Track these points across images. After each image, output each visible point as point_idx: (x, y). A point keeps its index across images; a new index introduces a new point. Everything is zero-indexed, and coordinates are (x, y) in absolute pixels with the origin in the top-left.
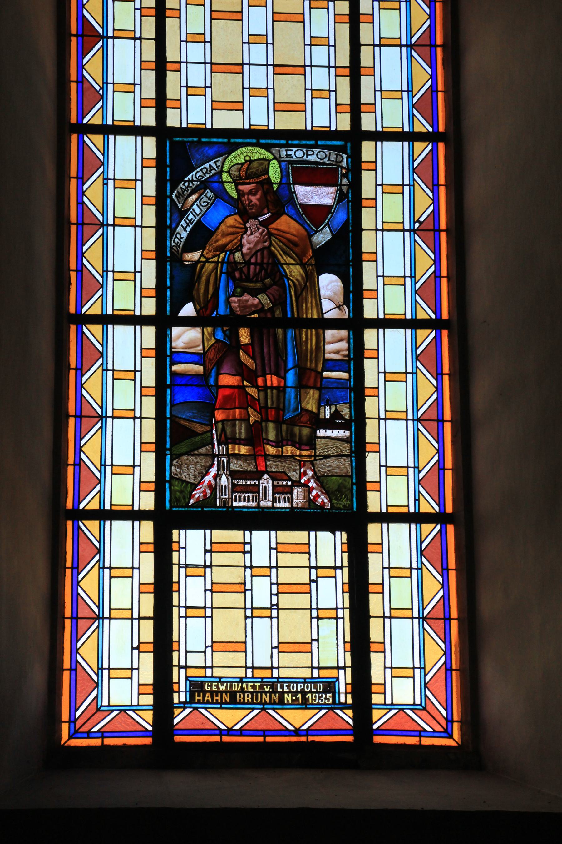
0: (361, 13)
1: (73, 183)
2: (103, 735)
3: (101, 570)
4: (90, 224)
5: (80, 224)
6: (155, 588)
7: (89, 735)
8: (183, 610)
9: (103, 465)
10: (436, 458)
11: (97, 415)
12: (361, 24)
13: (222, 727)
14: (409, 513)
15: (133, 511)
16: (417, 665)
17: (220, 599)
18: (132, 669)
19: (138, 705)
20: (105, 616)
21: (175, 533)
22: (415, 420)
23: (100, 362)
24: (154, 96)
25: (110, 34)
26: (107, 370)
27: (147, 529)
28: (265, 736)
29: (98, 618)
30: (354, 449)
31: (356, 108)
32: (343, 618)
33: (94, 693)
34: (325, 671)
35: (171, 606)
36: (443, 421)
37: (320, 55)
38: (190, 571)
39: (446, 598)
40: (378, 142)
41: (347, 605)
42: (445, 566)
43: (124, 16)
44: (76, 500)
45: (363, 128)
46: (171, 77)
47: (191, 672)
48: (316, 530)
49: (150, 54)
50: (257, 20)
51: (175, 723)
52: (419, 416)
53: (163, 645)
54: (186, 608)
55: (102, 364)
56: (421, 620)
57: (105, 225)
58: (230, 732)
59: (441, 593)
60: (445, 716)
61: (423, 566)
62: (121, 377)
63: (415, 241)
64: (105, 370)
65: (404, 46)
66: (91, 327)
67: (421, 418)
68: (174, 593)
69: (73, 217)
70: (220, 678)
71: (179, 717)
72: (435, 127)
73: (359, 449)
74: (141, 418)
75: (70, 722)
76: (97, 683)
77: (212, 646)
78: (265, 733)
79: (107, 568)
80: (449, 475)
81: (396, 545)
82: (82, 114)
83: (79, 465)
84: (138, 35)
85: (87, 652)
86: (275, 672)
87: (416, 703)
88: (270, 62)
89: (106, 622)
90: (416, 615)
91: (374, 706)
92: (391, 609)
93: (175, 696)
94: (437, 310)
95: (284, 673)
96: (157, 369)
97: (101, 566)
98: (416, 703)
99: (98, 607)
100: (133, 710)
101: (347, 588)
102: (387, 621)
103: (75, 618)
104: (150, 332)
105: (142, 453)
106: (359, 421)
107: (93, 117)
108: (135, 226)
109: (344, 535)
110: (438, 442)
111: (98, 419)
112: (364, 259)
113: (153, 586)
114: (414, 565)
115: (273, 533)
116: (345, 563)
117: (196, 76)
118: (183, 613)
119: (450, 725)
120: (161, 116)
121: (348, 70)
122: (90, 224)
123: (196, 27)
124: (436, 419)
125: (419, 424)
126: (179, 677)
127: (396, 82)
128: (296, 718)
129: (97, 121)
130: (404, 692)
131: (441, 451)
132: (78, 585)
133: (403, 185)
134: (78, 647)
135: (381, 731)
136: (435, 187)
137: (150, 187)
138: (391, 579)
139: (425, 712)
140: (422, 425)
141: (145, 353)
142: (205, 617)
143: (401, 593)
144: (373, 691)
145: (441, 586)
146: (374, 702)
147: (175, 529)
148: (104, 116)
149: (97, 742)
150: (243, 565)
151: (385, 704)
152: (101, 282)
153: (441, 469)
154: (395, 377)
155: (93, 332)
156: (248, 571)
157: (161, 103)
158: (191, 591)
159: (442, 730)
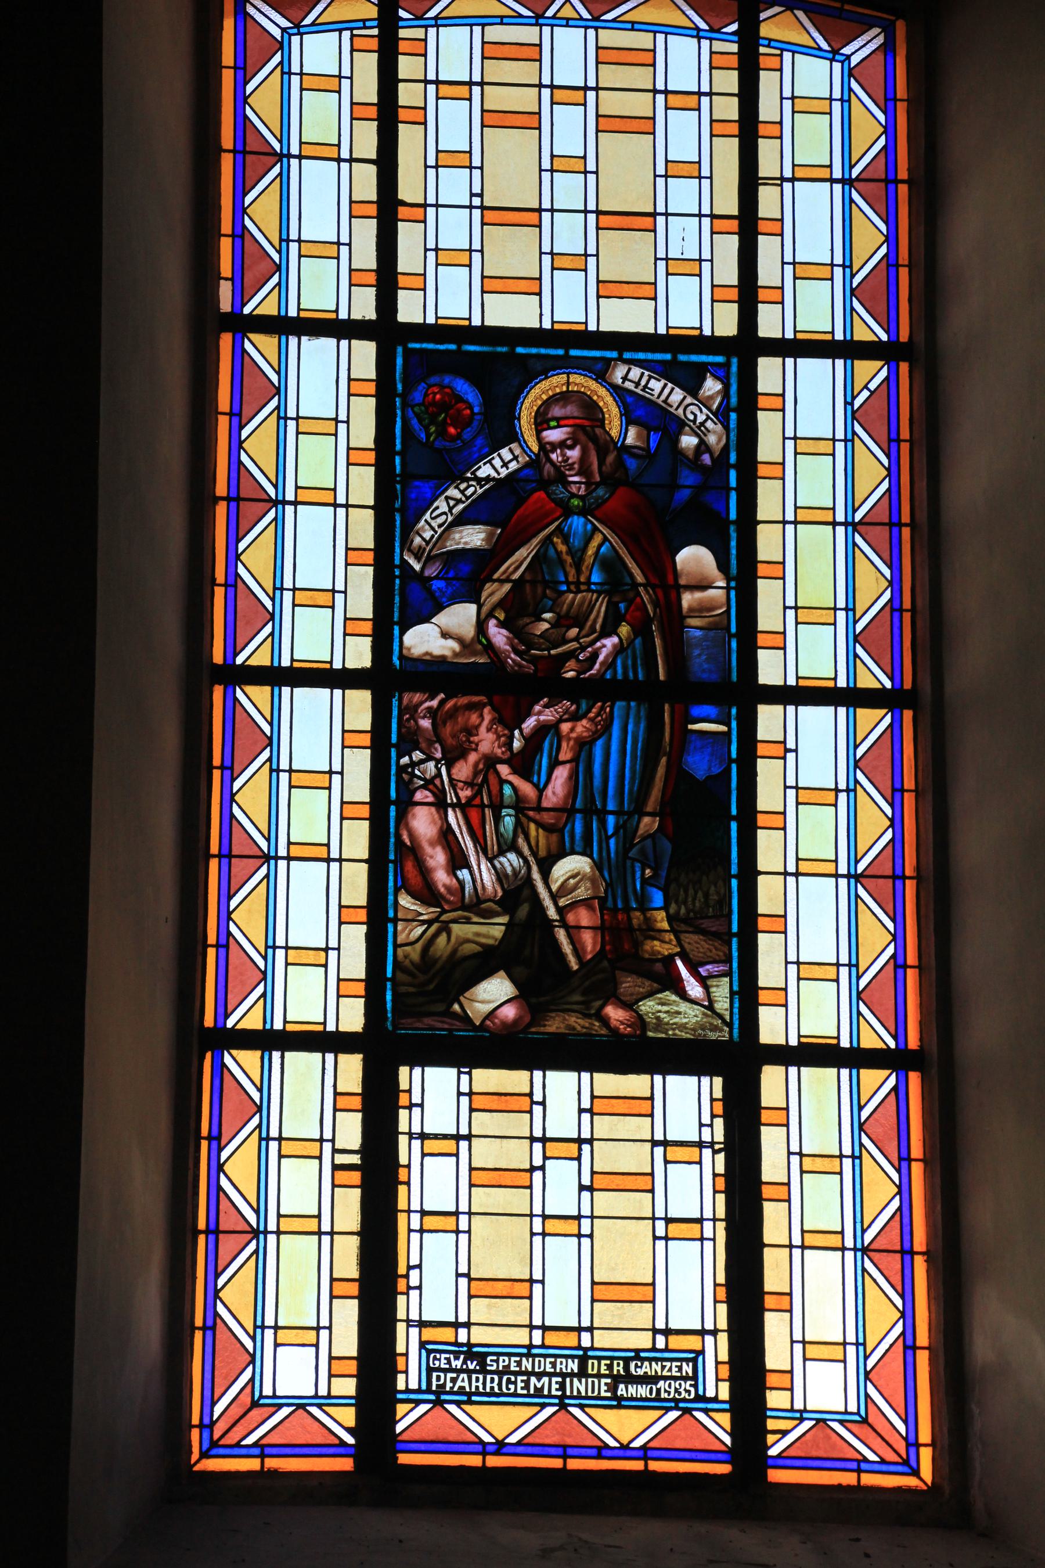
2: (262, 1451)
3: (264, 1143)
4: (258, 156)
5: (234, 499)
7: (237, 1450)
8: (415, 1218)
9: (284, 240)
13: (487, 1438)
14: (836, 689)
16: (851, 1338)
21: (404, 1071)
22: (859, 1250)
23: (266, 754)
24: (373, 265)
25: (290, 496)
27: (351, 1069)
28: (565, 1457)
31: (748, 293)
34: (681, 1338)
36: (912, 1253)
37: (683, 195)
38: (431, 1146)
39: (904, 1213)
41: (721, 1213)
42: (893, 435)
44: (230, 650)
45: (761, 334)
46: (408, 236)
47: (429, 1334)
48: (664, 1073)
51: (398, 1431)
53: (379, 1281)
55: (270, 759)
56: (859, 1254)
58: (500, 1447)
59: (896, 1203)
60: (904, 1434)
61: (858, 786)
63: (855, 544)
65: (837, 181)
67: (872, 1247)
71: (407, 1418)
73: (744, 574)
74: (347, 506)
76: (253, 1356)
78: (564, 1451)
79: (274, 1139)
80: (923, 1359)
81: (811, 1113)
82: (241, 297)
83: (227, 946)
84: (341, 499)
85: (236, 1294)
88: (592, 206)
89: (282, 864)
90: (849, 1243)
91: (769, 1413)
92: (803, 1231)
93: (401, 1379)
95: (603, 1339)
96: (379, 236)
97: (264, 1135)
99: (260, 1090)
100: (319, 1406)
101: (721, 1183)
102: (797, 1252)
103: (240, 152)
107: (262, 303)
108: (339, 160)
109: (718, 1081)
111: (251, 1236)
114: (842, 785)
115: (585, 1076)
116: (723, 1323)
118: (415, 1224)
119: (912, 1450)
120: (387, 301)
121: (736, 222)
122: (251, 502)
123: (454, 138)
124: (887, 521)
126: (407, 1341)
128: (626, 1427)
129: (262, 659)
130: (826, 1388)
132: (232, 799)
133: (845, 1344)
134: (248, 93)
135: (784, 1461)
137: (358, 784)
140: (872, 1261)
141: (358, 209)
142: (457, 1232)
143: (822, 1202)
146: (770, 1404)
147: (404, 1065)
148: (276, 650)
150: (528, 1135)
151: (792, 1410)
154: (814, 616)
155: (260, 348)
157: (387, 279)
158: (431, 1182)
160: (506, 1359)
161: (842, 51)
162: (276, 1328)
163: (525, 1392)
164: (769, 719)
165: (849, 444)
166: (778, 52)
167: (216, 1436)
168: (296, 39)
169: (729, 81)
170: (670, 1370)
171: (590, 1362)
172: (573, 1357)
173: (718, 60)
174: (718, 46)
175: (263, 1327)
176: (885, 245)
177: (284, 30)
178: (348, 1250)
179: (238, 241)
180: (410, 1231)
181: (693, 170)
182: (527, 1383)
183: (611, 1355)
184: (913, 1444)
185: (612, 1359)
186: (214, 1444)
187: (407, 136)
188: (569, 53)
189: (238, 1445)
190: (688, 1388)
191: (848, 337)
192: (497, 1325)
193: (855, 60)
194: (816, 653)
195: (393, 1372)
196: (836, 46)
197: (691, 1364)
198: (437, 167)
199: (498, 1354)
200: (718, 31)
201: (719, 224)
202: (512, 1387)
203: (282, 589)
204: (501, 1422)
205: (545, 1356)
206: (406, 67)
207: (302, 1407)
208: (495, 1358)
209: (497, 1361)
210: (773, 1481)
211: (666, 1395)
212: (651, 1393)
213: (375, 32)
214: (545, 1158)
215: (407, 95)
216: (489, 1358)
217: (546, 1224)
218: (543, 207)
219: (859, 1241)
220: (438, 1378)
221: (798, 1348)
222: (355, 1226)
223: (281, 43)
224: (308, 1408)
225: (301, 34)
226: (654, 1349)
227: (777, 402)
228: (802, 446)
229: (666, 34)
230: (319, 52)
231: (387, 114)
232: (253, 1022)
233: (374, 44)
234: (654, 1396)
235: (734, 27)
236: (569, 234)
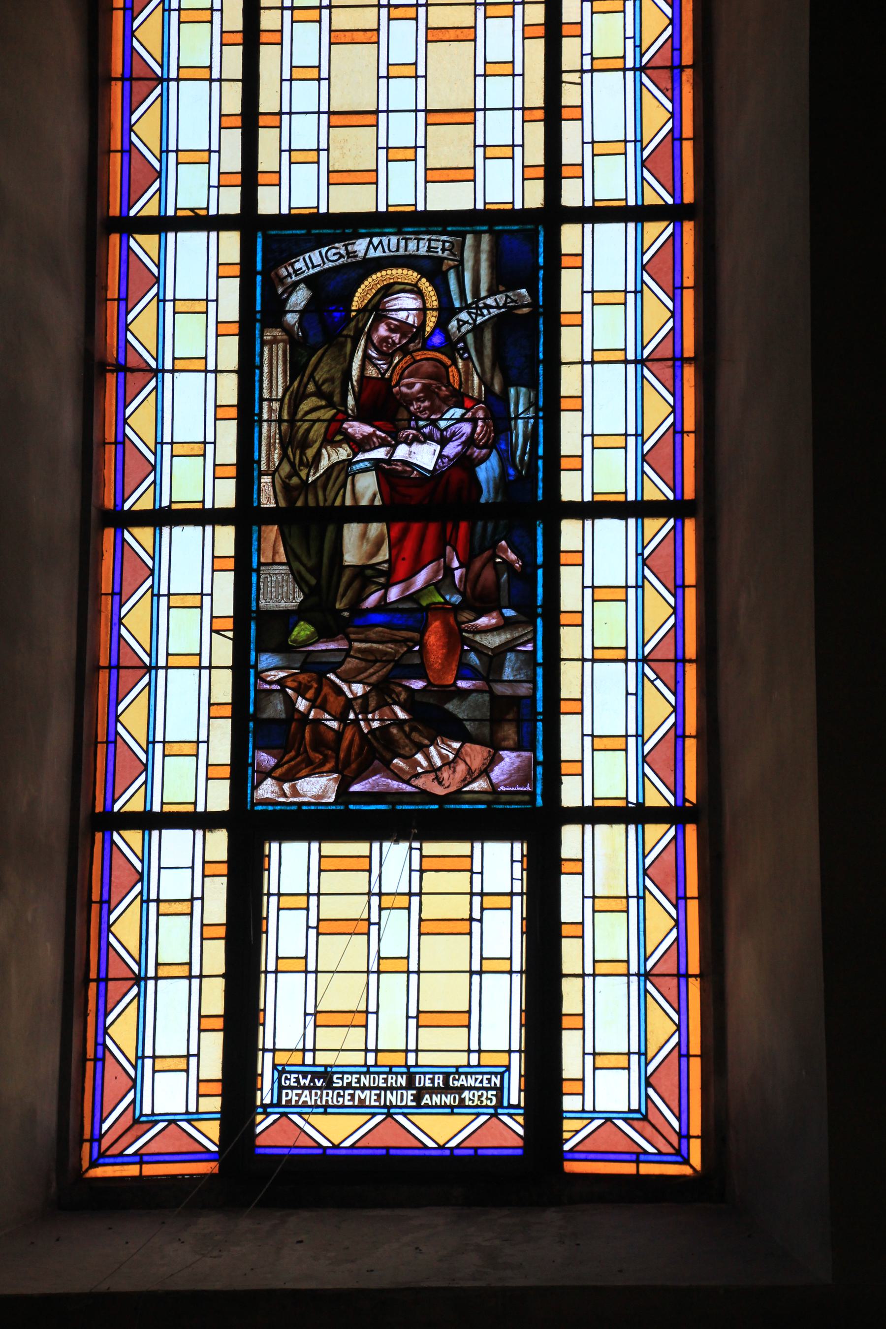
4: (144, 81)
6: (228, 932)
7: (121, 1159)
10: (672, 720)
11: (142, 665)
12: (562, 568)
15: (204, 510)
18: (188, 1056)
19: (197, 1112)
20: (171, 77)
22: (642, 975)
31: (553, 171)
33: (130, 1097)
37: (499, 91)
43: (194, 45)
46: (267, 139)
49: (233, 101)
50: (402, 40)
52: (648, 969)
56: (642, 979)
60: (677, 1130)
62: (183, 602)
65: (631, 362)
66: (136, 531)
67: (650, 657)
72: (678, 194)
73: (551, 408)
77: (317, 928)
81: (601, 859)
86: (411, 1057)
94: (676, 189)
100: (189, 1121)
108: (200, 668)
110: (673, 395)
113: (224, 928)
117: (305, 132)
120: (249, 198)
122: (666, 362)
125: (646, 666)
127: (618, 130)
131: (676, 21)
133: (627, 897)
136: (678, 589)
138: (596, 914)
139: (646, 1124)
143: (611, 937)
145: (671, 611)
146: (566, 1107)
149: (132, 1170)
152: (158, 169)
153: (680, 736)
157: (250, 178)
158: (285, 933)
159: (672, 1151)
160: (349, 1076)
162: (154, 1057)
163: (377, 1104)
164: (571, 533)
170: (481, 1082)
171: (417, 1076)
172: (402, 1074)
175: (143, 1057)
181: (510, 70)
182: (352, 1096)
183: (432, 1071)
184: (684, 1136)
185: (434, 1073)
186: (102, 1155)
187: (268, 55)
189: (121, 1155)
190: (489, 1096)
191: (640, 203)
192: (339, 1047)
194: (608, 473)
197: (499, 1077)
198: (291, 80)
199: (343, 1073)
202: (341, 1099)
205: (379, 1073)
208: (340, 1076)
209: (342, 1079)
211: (471, 1103)
212: (454, 1102)
214: (483, 909)
216: (335, 1076)
220: (287, 1095)
222: (222, 970)
224: (179, 1123)
226: (469, 1066)
228: (598, 298)
234: (457, 1103)
236: (402, 130)
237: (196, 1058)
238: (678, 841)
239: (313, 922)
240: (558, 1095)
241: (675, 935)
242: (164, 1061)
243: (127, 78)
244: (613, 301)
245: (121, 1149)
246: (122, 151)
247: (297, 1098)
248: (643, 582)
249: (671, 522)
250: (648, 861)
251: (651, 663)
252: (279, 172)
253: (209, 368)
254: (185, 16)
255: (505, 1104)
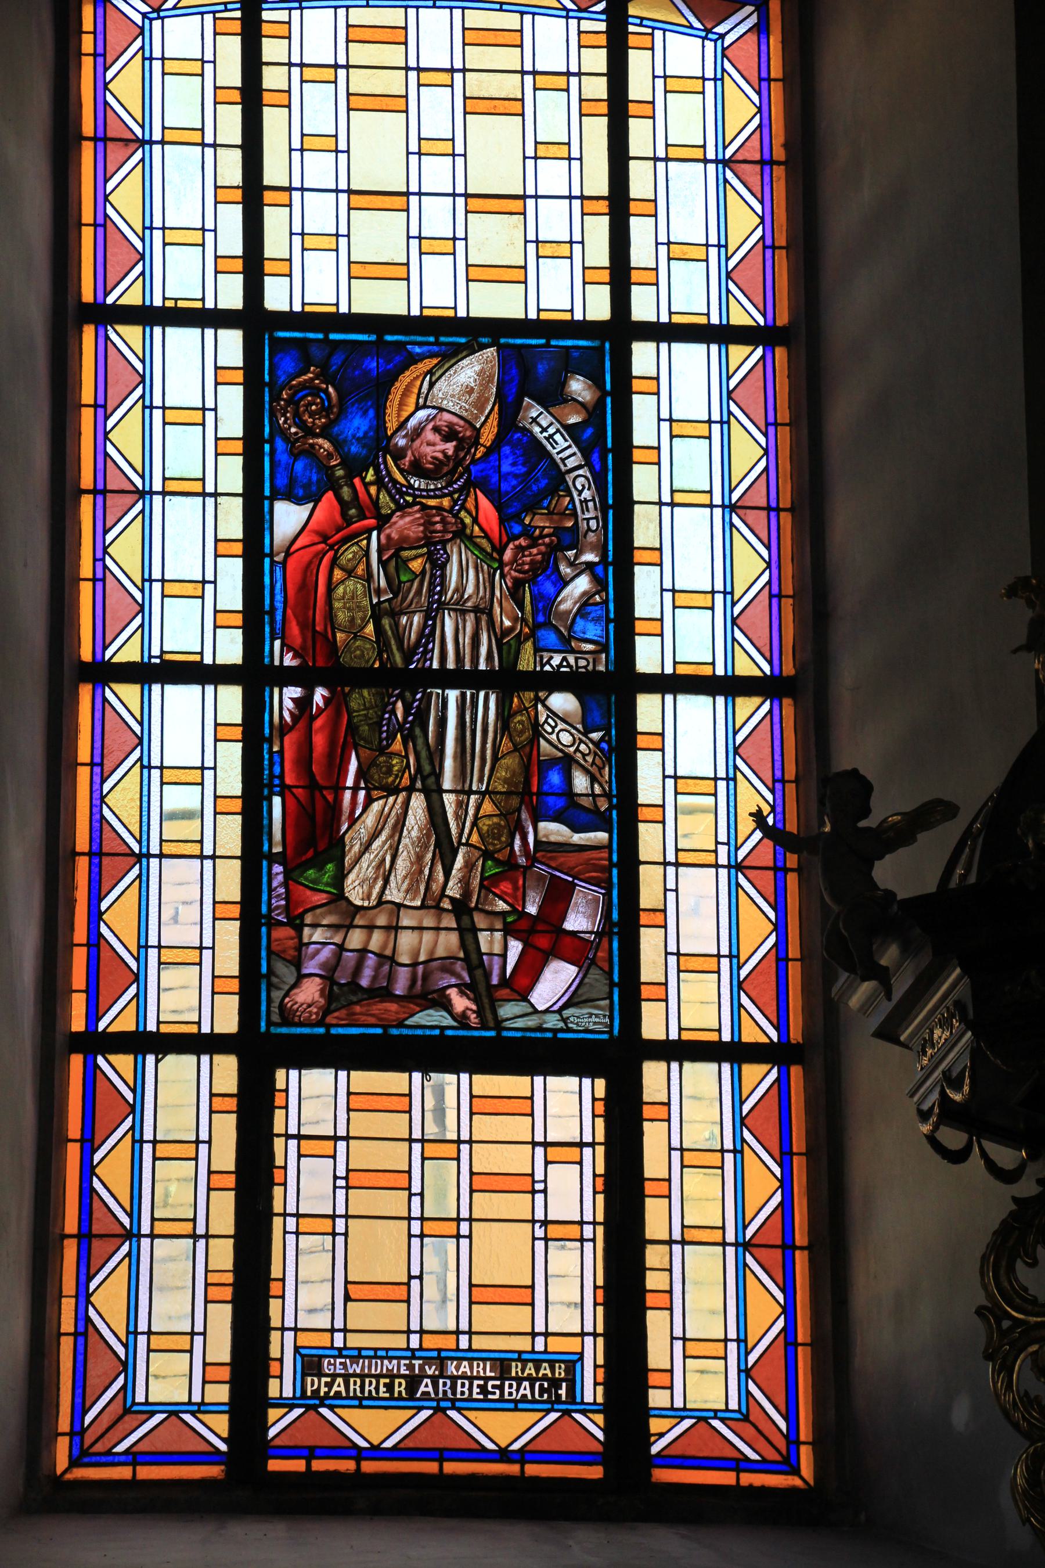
0: (637, 616)
1: (73, 1151)
4: (104, 1236)
7: (109, 1459)
8: (291, 1223)
11: (134, 489)
17: (362, 1201)
26: (151, 407)
27: (226, 1070)
29: (142, 494)
30: (615, 916)
31: (620, 275)
32: (594, 1240)
35: (270, 1214)
37: (553, 176)
40: (661, 345)
44: (78, 1408)
46: (274, 220)
53: (251, 1287)
54: (298, 1215)
55: (143, 397)
56: (740, 1250)
57: (135, 1236)
58: (376, 1452)
63: (738, 885)
64: (147, 407)
67: (745, 864)
68: (275, 1187)
69: (82, 843)
70: (360, 1349)
73: (620, 562)
75: (71, 1434)
78: (441, 1455)
81: (694, 1106)
84: (209, 139)
87: (731, 1407)
89: (157, 500)
90: (730, 1237)
98: (731, 1407)
99: (134, 1091)
100: (193, 1414)
101: (600, 1108)
103: (85, 1236)
104: (227, 1066)
105: (218, 559)
106: (629, 860)
109: (601, 1084)
112: (630, 44)
114: (709, 74)
117: (320, 213)
120: (254, 289)
125: (740, 875)
126: (282, 1347)
127: (702, 234)
128: (503, 1429)
133: (713, 592)
135: (666, 1460)
137: (229, 960)
144: (649, 1304)
145: (759, 221)
149: (123, 1473)
156: (417, 1147)
157: (253, 265)
158: (307, 1184)
161: (715, 30)
165: (719, 83)
166: (650, 31)
167: (86, 1445)
168: (157, 24)
169: (597, 60)
173: (586, 40)
174: (586, 25)
176: (774, 934)
177: (144, 15)
178: (223, 1254)
179: (100, 230)
180: (285, 1232)
187: (273, 119)
188: (435, 34)
189: (109, 1453)
192: (375, 1322)
193: (729, 40)
195: (265, 1376)
196: (709, 26)
200: (585, 10)
201: (590, 206)
203: (151, 228)
204: (376, 1427)
206: (271, 49)
207: (175, 1414)
210: (641, 671)
213: (238, 14)
215: (272, 78)
217: (422, 1228)
218: (411, 190)
219: (740, 1234)
221: (676, 1155)
223: (142, 28)
225: (163, 18)
227: (649, 208)
229: (534, 14)
230: (181, 36)
231: (252, 97)
232: (133, 298)
233: (237, 26)
235: (601, 6)
237: (202, 1337)
238: (782, 1083)
239: (341, 1172)
240: (643, 1388)
241: (761, 234)
242: (163, 1331)
243: (101, 139)
244: (696, 434)
245: (109, 1446)
246: (95, 225)
247: (326, 1389)
248: (723, 75)
249: (759, 351)
250: (746, 1108)
251: (747, 872)
252: (290, 260)
253: (207, 491)
254: (156, 1342)
255: (578, 1400)
